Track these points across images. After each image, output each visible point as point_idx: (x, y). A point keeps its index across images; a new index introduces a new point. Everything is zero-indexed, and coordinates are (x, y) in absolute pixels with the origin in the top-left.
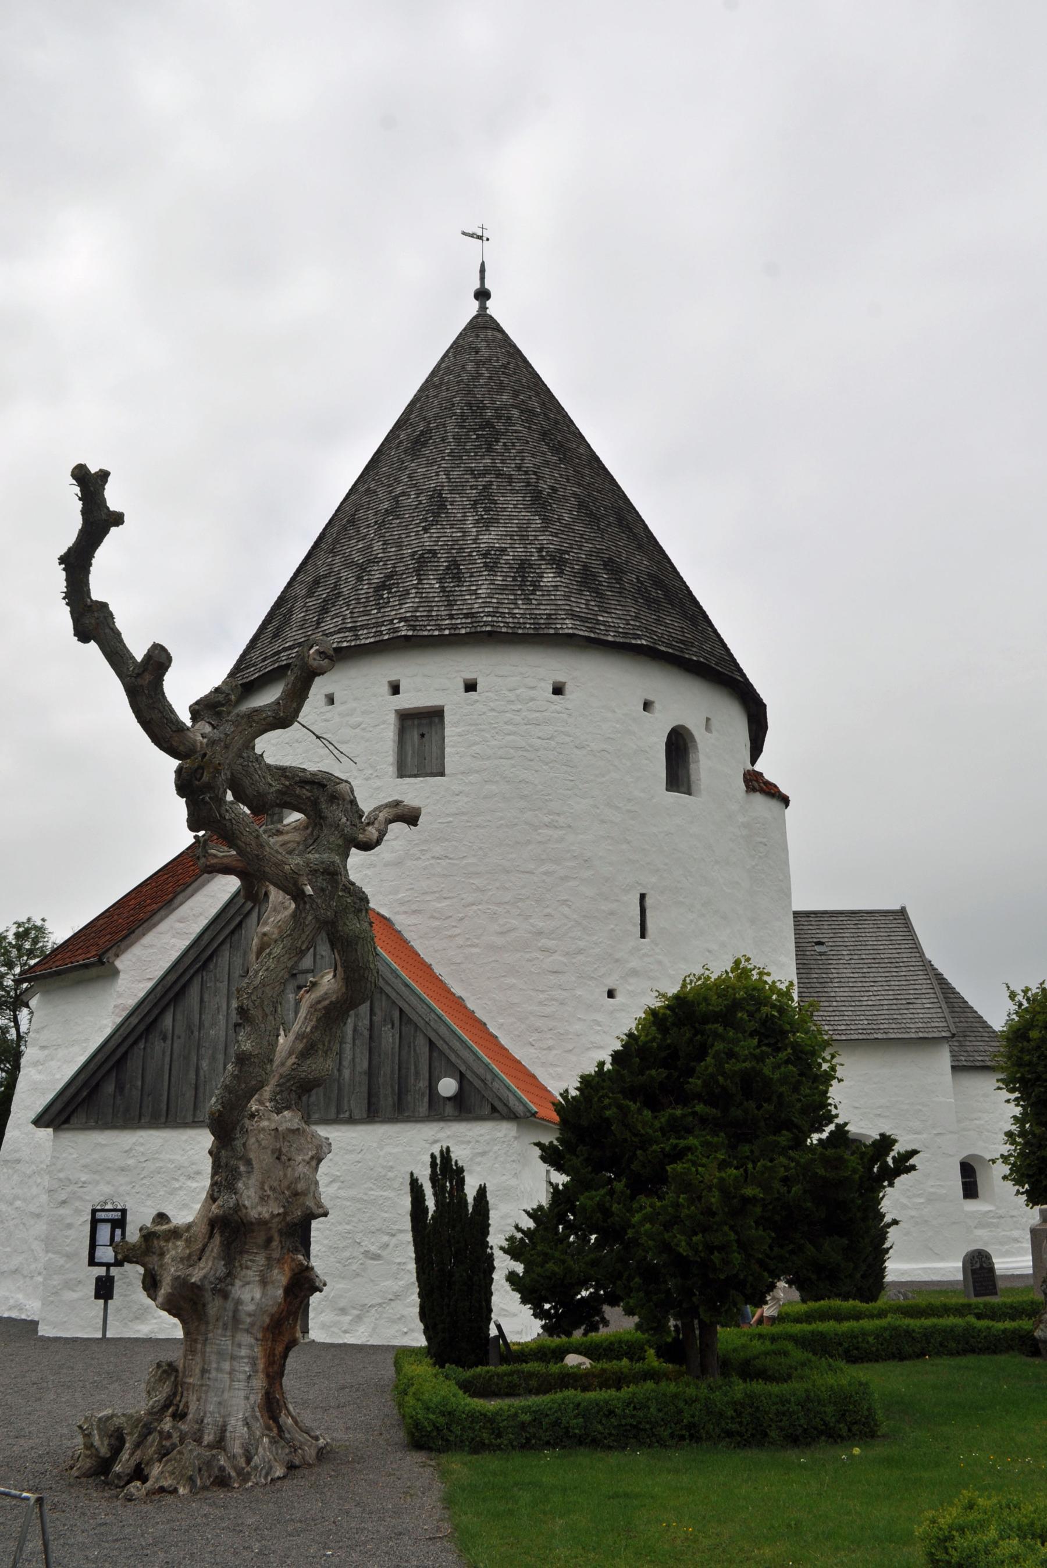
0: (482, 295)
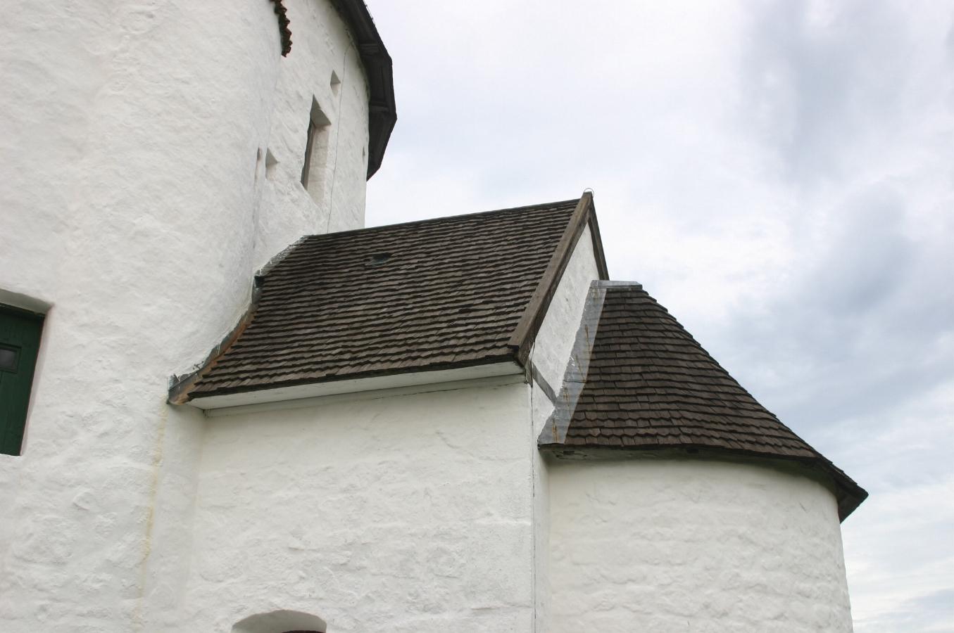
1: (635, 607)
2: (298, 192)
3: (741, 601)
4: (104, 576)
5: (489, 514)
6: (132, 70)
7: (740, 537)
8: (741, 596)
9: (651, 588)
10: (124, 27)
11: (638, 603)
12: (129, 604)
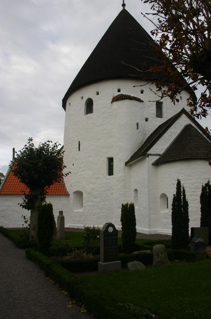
0: (124, 5)
2: (156, 119)
4: (121, 187)
7: (177, 173)
9: (166, 182)
12: (124, 190)
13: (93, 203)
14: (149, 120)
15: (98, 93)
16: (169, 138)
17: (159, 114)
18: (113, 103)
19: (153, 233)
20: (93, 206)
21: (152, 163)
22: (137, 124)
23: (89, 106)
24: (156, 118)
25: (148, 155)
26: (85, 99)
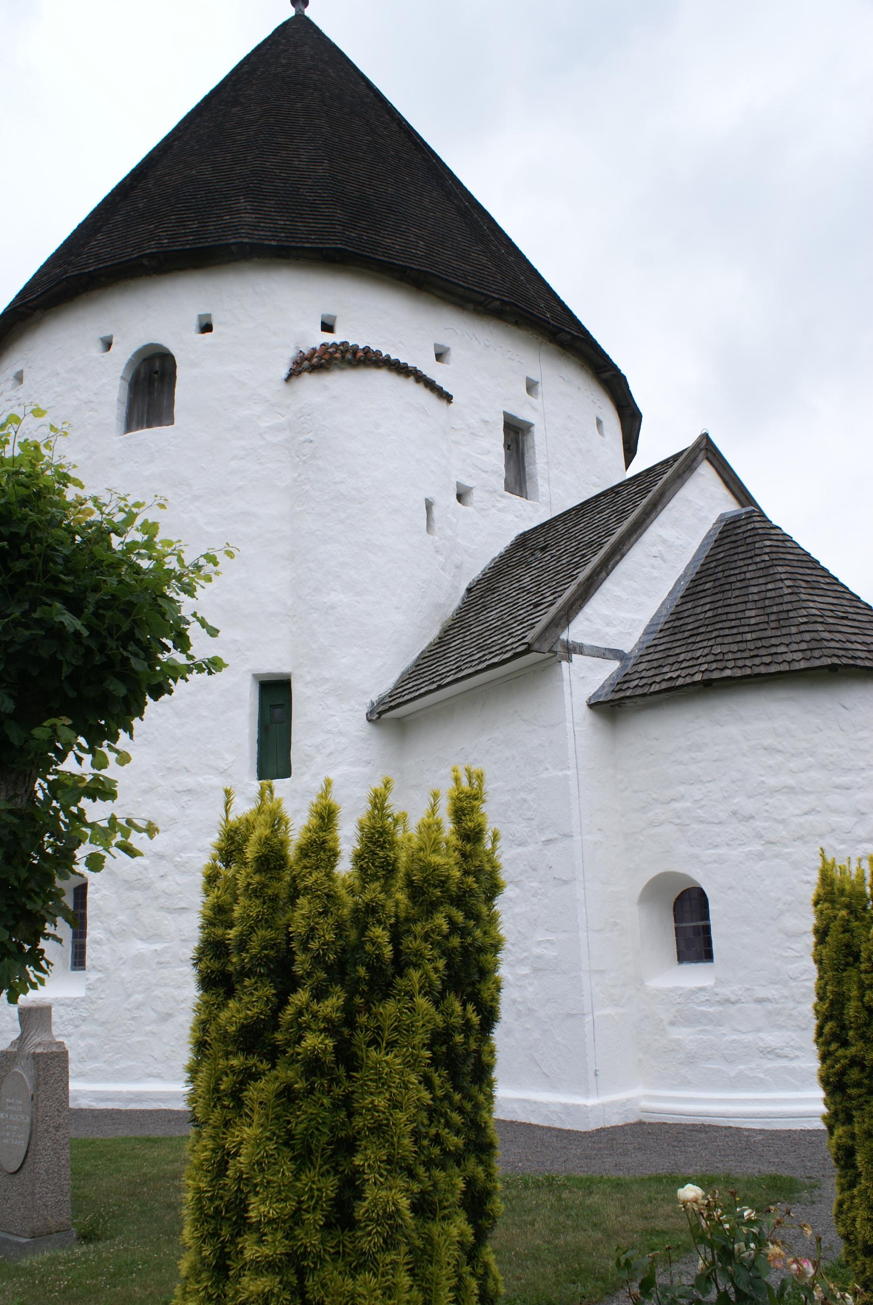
1: (677, 821)
2: (504, 501)
3: (767, 804)
5: (547, 769)
6: (307, 487)
8: (767, 800)
9: (689, 804)
10: (298, 457)
11: (679, 817)
13: (158, 947)
14: (476, 496)
15: (205, 322)
16: (655, 573)
17: (518, 479)
18: (294, 379)
19: (616, 1120)
20: (159, 963)
21: (586, 698)
22: (429, 505)
23: (152, 386)
24: (502, 496)
25: (571, 649)
26: (124, 352)
